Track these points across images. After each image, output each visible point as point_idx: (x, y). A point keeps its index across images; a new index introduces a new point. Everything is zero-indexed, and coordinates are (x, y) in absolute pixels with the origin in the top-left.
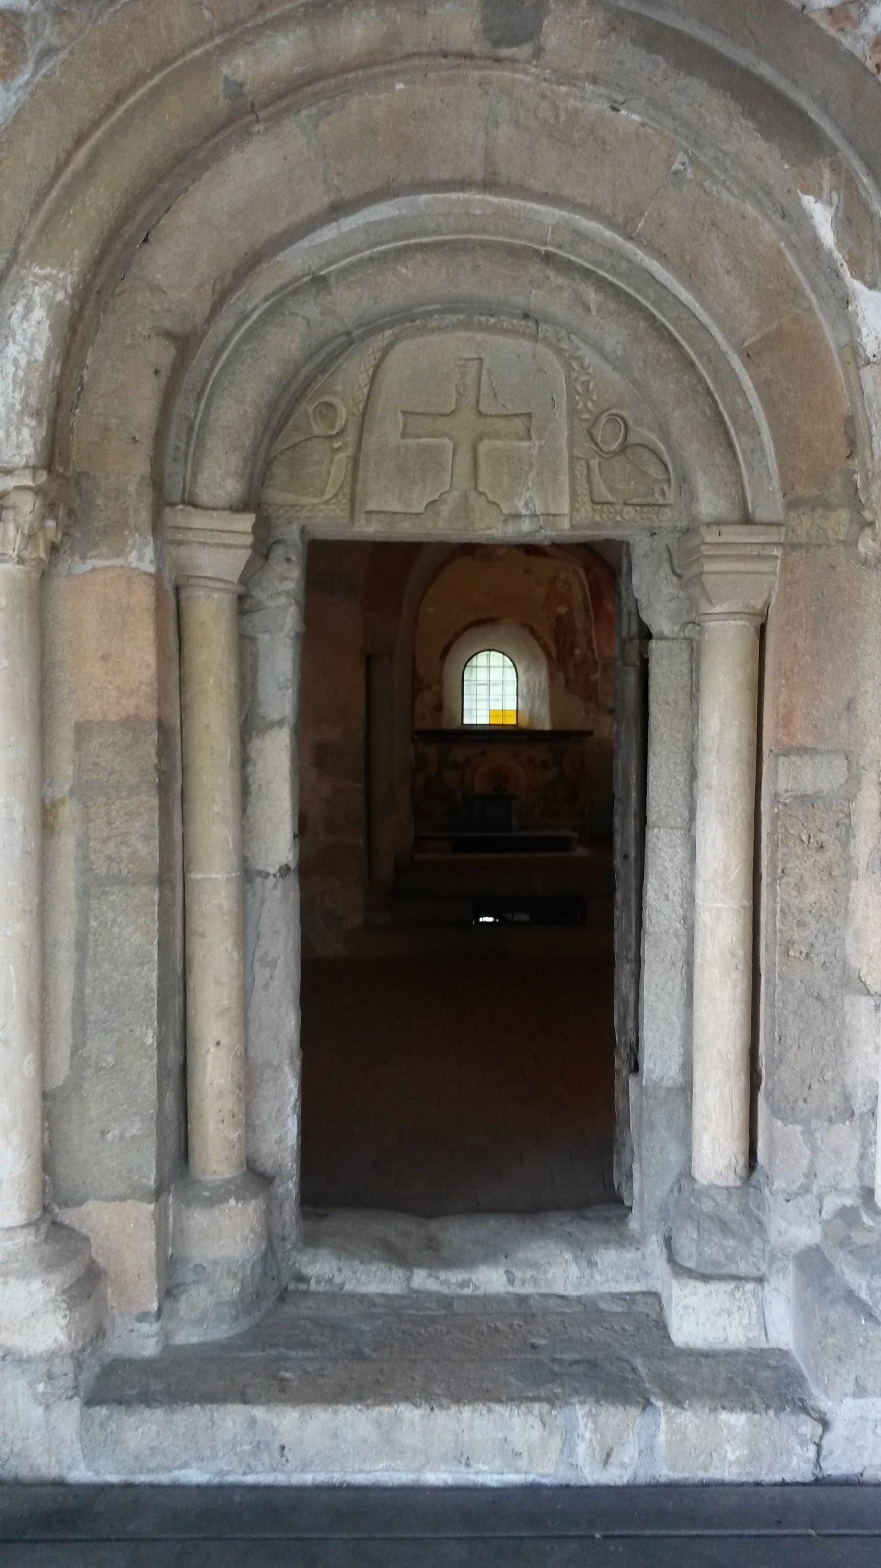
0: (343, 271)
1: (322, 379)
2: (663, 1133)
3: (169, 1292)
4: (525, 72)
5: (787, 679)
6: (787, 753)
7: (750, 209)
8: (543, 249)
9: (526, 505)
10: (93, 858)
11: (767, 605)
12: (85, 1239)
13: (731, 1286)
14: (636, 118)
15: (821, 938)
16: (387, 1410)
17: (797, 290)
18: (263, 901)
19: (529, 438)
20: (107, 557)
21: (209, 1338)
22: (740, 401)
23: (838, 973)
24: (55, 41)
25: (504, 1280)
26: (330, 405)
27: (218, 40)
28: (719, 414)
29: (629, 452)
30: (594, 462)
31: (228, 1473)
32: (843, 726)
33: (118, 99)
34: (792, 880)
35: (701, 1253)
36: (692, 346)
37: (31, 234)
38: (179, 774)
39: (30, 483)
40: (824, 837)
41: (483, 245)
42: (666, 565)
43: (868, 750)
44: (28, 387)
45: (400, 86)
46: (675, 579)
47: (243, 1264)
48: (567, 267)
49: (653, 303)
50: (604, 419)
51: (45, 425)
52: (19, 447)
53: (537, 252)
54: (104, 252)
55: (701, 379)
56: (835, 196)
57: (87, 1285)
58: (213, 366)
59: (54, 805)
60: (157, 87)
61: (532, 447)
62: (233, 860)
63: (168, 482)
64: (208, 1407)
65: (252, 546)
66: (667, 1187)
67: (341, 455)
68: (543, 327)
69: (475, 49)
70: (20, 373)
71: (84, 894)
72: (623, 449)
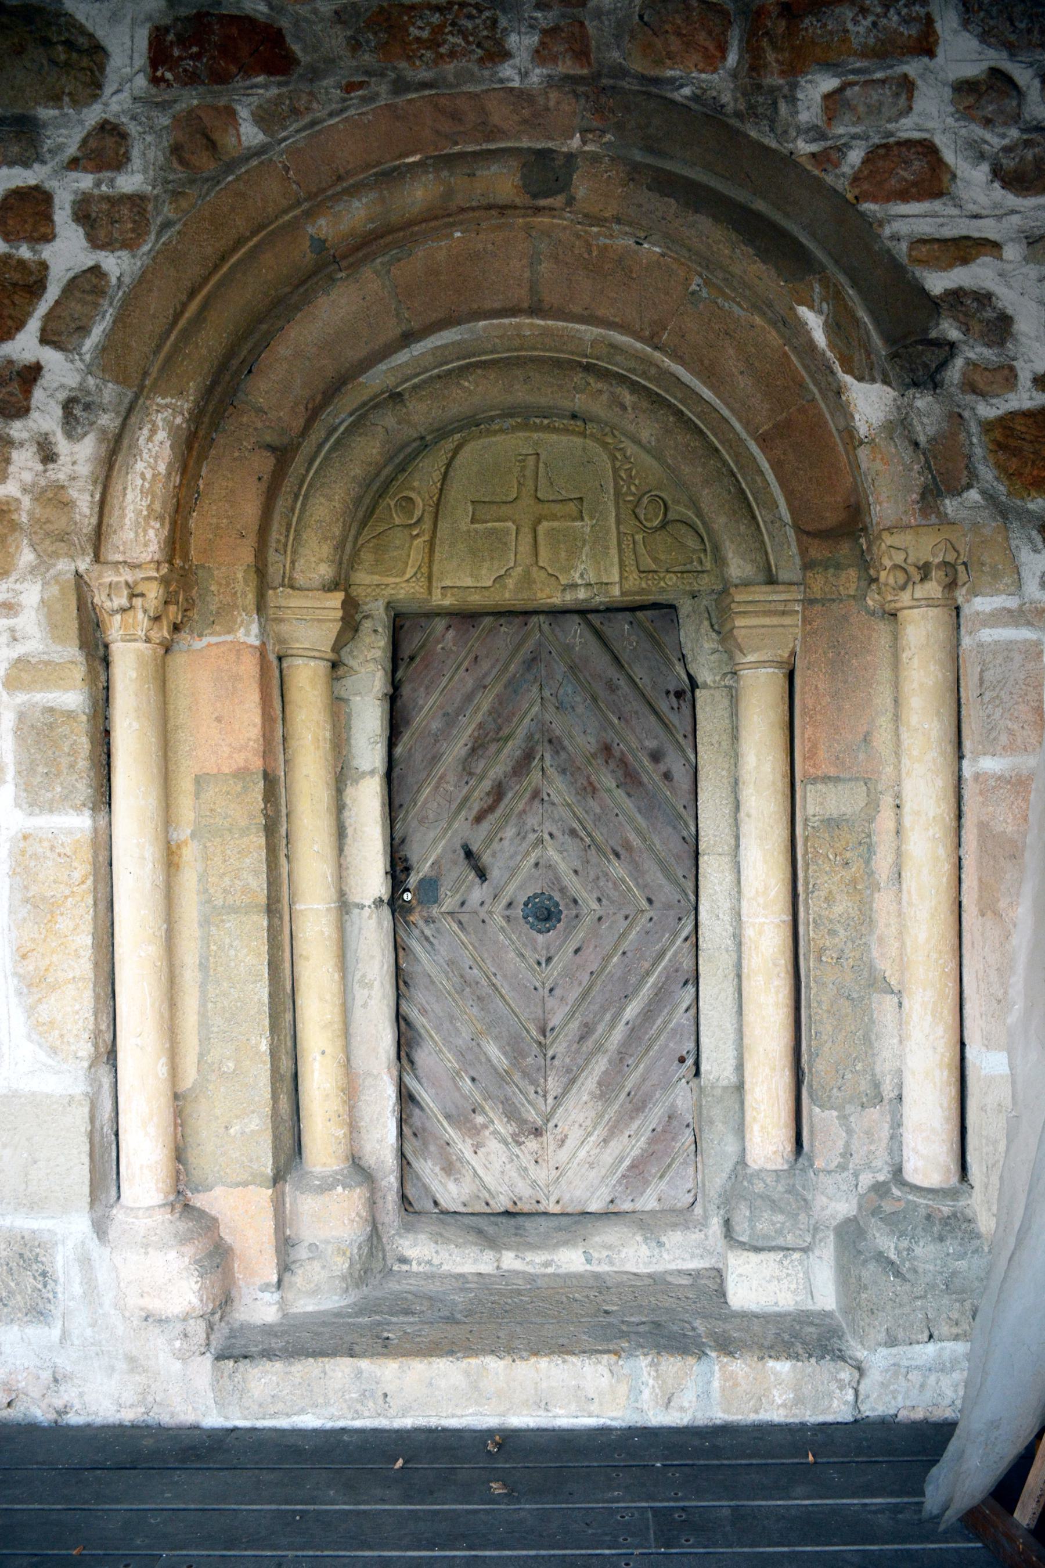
0: (415, 387)
1: (401, 478)
2: (720, 1126)
3: (285, 1268)
4: (561, 218)
5: (811, 717)
6: (814, 781)
7: (758, 320)
8: (585, 360)
9: (582, 575)
10: (211, 891)
11: (793, 654)
12: (215, 1220)
13: (781, 1255)
14: (657, 250)
15: (849, 944)
16: (474, 1361)
17: (801, 385)
18: (360, 929)
19: (582, 519)
20: (220, 635)
21: (322, 1308)
22: (758, 479)
23: (866, 974)
24: (171, 215)
25: (583, 1260)
26: (410, 500)
27: (306, 206)
28: (742, 492)
29: (669, 528)
30: (639, 537)
31: (339, 1419)
32: (862, 756)
33: (223, 258)
34: (823, 894)
35: (753, 1228)
36: (715, 435)
37: (154, 371)
38: (284, 819)
39: (155, 574)
40: (848, 855)
41: (533, 360)
42: (706, 623)
43: (884, 777)
44: (153, 497)
45: (458, 234)
46: (714, 635)
47: (351, 1244)
48: (604, 374)
49: (680, 401)
50: (645, 500)
51: (167, 526)
52: (146, 545)
53: (580, 363)
54: (215, 383)
55: (725, 463)
56: (825, 306)
57: (217, 1259)
58: (308, 471)
59: (179, 847)
60: (255, 246)
61: (584, 527)
62: (332, 893)
63: (271, 570)
64: (320, 1360)
65: (343, 619)
66: (725, 1175)
67: (420, 540)
68: (589, 425)
69: (518, 201)
70: (147, 485)
71: (205, 922)
72: (663, 526)
